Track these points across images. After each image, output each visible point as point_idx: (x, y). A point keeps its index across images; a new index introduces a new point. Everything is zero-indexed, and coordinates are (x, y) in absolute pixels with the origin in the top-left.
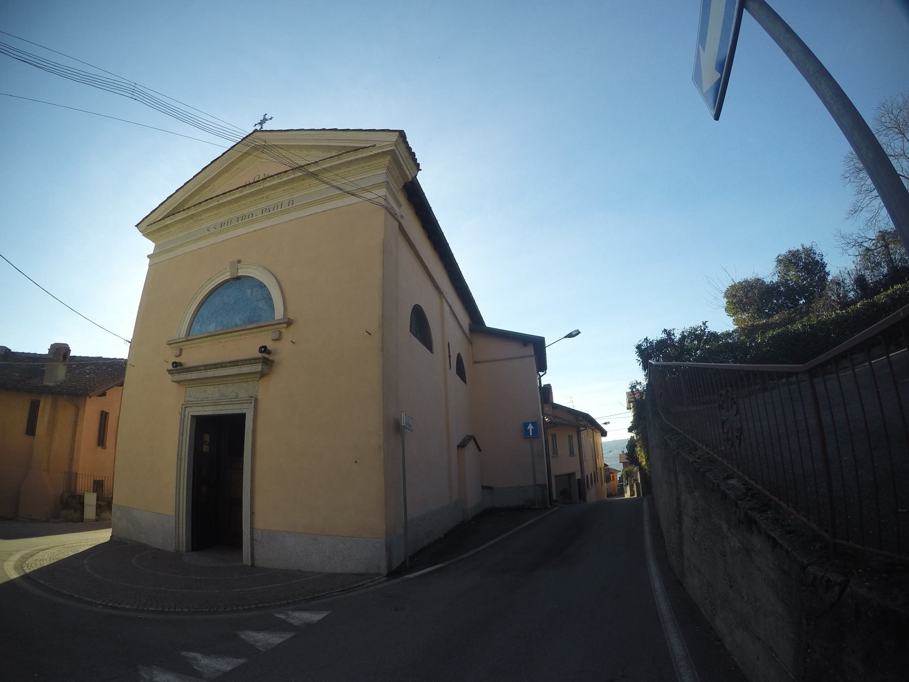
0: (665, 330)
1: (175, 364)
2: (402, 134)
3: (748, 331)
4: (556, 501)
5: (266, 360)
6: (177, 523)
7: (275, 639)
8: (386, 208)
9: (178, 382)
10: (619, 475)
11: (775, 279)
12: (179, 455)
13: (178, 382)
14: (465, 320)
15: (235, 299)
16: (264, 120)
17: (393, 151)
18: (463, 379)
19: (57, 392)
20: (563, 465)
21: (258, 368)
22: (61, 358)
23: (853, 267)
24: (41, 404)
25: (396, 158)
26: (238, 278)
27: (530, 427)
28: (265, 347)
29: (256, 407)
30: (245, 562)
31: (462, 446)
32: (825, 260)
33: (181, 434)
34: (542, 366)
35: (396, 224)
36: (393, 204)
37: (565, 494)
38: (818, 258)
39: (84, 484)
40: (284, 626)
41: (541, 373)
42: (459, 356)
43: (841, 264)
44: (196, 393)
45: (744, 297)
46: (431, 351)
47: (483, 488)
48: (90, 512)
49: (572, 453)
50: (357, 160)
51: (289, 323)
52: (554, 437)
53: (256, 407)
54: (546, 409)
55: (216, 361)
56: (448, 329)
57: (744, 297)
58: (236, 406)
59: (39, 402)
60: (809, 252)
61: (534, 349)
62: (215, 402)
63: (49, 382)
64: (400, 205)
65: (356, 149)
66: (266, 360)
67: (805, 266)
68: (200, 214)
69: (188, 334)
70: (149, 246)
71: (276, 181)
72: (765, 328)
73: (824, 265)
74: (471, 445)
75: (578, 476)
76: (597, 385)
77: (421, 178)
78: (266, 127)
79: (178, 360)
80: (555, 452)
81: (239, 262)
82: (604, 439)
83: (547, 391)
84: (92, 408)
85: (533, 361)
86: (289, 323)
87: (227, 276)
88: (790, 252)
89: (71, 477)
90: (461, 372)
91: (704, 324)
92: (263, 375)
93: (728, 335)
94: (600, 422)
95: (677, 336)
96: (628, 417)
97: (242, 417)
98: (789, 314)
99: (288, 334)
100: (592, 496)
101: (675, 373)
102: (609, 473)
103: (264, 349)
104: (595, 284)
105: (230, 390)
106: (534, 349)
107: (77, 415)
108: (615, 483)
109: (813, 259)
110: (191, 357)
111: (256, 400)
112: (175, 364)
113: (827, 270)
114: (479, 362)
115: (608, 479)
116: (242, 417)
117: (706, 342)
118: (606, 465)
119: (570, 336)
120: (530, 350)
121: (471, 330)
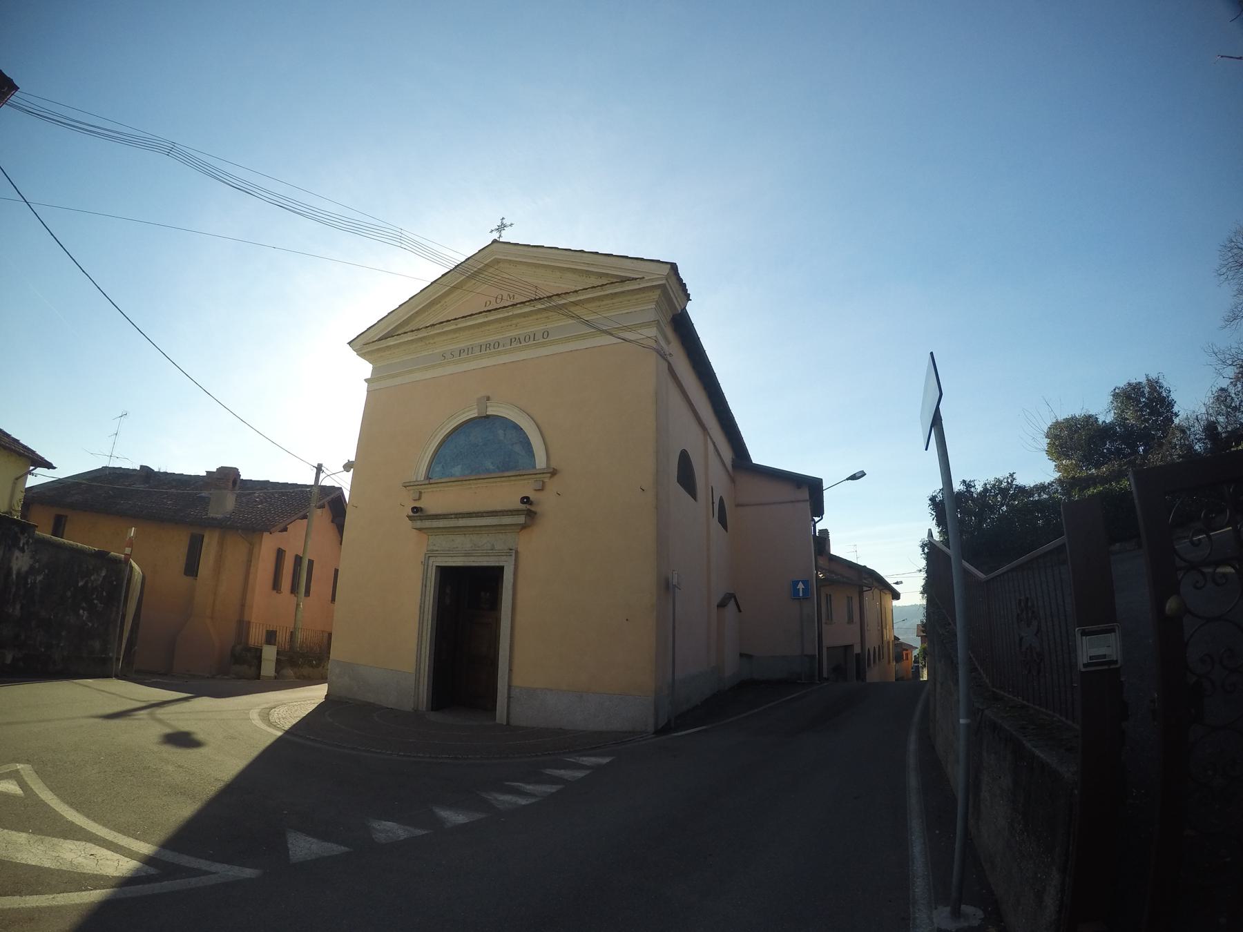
0: (964, 482)
1: (416, 510)
2: (674, 267)
3: (1068, 484)
4: (827, 679)
5: (529, 511)
6: (417, 681)
7: (579, 774)
8: (658, 352)
9: (420, 529)
10: (915, 652)
11: (1109, 418)
12: (422, 608)
13: (420, 529)
14: (728, 455)
15: (483, 444)
16: (501, 228)
17: (664, 285)
18: (725, 527)
19: (225, 526)
20: (839, 633)
21: (521, 519)
22: (230, 484)
23: (1204, 411)
24: (206, 540)
25: (667, 289)
26: (488, 417)
27: (801, 586)
28: (528, 498)
29: (516, 560)
30: (498, 721)
31: (722, 605)
32: (1173, 396)
33: (424, 586)
34: (818, 510)
35: (666, 365)
36: (663, 343)
37: (839, 671)
38: (1164, 394)
39: (256, 636)
40: (554, 780)
41: (817, 519)
42: (721, 500)
43: (1192, 401)
44: (441, 542)
45: (1071, 439)
46: (695, 498)
47: (741, 655)
48: (268, 668)
49: (851, 620)
50: (623, 292)
51: (554, 473)
52: (829, 597)
53: (516, 560)
54: (822, 562)
55: (471, 510)
56: (712, 473)
57: (1071, 439)
58: (492, 559)
59: (203, 537)
60: (1154, 385)
61: (811, 492)
62: (463, 552)
63: (214, 513)
64: (668, 343)
65: (624, 280)
66: (529, 511)
67: (1147, 403)
68: (433, 336)
69: (428, 477)
70: (365, 368)
71: (527, 309)
72: (1090, 481)
73: (1171, 404)
74: (732, 604)
75: (857, 650)
76: (884, 535)
77: (691, 309)
78: (507, 236)
79: (417, 504)
80: (1104, 656)
81: (488, 399)
82: (895, 603)
83: (823, 540)
84: (268, 545)
85: (807, 506)
86: (554, 473)
87: (473, 414)
88: (1129, 384)
89: (243, 627)
90: (723, 520)
91: (1011, 475)
92: (524, 527)
93: (1041, 488)
94: (890, 581)
95: (979, 488)
96: (920, 580)
97: (500, 569)
98: (1120, 466)
99: (553, 485)
100: (873, 675)
101: (975, 529)
102: (901, 649)
103: (526, 500)
104: (889, 411)
105: (485, 541)
106: (811, 492)
107: (250, 553)
108: (908, 664)
109: (1160, 394)
110: (434, 502)
111: (517, 552)
112: (416, 510)
113: (1175, 409)
114: (742, 505)
115: (899, 658)
116: (500, 569)
117: (1014, 497)
118: (896, 639)
119: (853, 477)
120: (805, 494)
121: (734, 466)
